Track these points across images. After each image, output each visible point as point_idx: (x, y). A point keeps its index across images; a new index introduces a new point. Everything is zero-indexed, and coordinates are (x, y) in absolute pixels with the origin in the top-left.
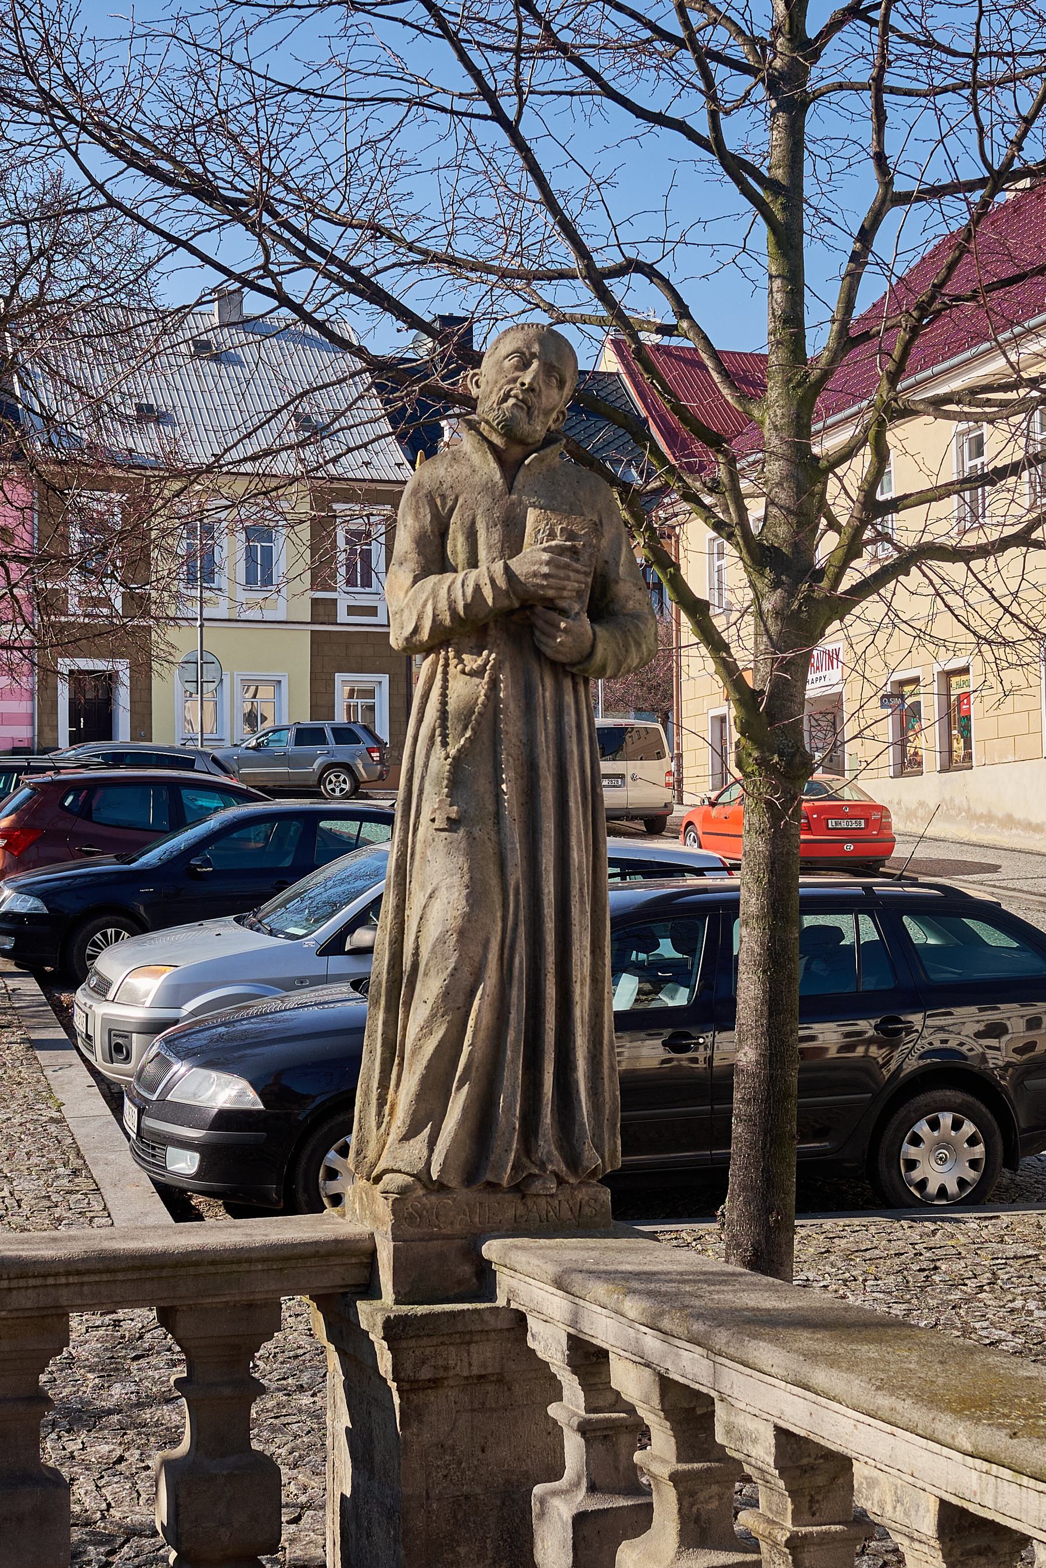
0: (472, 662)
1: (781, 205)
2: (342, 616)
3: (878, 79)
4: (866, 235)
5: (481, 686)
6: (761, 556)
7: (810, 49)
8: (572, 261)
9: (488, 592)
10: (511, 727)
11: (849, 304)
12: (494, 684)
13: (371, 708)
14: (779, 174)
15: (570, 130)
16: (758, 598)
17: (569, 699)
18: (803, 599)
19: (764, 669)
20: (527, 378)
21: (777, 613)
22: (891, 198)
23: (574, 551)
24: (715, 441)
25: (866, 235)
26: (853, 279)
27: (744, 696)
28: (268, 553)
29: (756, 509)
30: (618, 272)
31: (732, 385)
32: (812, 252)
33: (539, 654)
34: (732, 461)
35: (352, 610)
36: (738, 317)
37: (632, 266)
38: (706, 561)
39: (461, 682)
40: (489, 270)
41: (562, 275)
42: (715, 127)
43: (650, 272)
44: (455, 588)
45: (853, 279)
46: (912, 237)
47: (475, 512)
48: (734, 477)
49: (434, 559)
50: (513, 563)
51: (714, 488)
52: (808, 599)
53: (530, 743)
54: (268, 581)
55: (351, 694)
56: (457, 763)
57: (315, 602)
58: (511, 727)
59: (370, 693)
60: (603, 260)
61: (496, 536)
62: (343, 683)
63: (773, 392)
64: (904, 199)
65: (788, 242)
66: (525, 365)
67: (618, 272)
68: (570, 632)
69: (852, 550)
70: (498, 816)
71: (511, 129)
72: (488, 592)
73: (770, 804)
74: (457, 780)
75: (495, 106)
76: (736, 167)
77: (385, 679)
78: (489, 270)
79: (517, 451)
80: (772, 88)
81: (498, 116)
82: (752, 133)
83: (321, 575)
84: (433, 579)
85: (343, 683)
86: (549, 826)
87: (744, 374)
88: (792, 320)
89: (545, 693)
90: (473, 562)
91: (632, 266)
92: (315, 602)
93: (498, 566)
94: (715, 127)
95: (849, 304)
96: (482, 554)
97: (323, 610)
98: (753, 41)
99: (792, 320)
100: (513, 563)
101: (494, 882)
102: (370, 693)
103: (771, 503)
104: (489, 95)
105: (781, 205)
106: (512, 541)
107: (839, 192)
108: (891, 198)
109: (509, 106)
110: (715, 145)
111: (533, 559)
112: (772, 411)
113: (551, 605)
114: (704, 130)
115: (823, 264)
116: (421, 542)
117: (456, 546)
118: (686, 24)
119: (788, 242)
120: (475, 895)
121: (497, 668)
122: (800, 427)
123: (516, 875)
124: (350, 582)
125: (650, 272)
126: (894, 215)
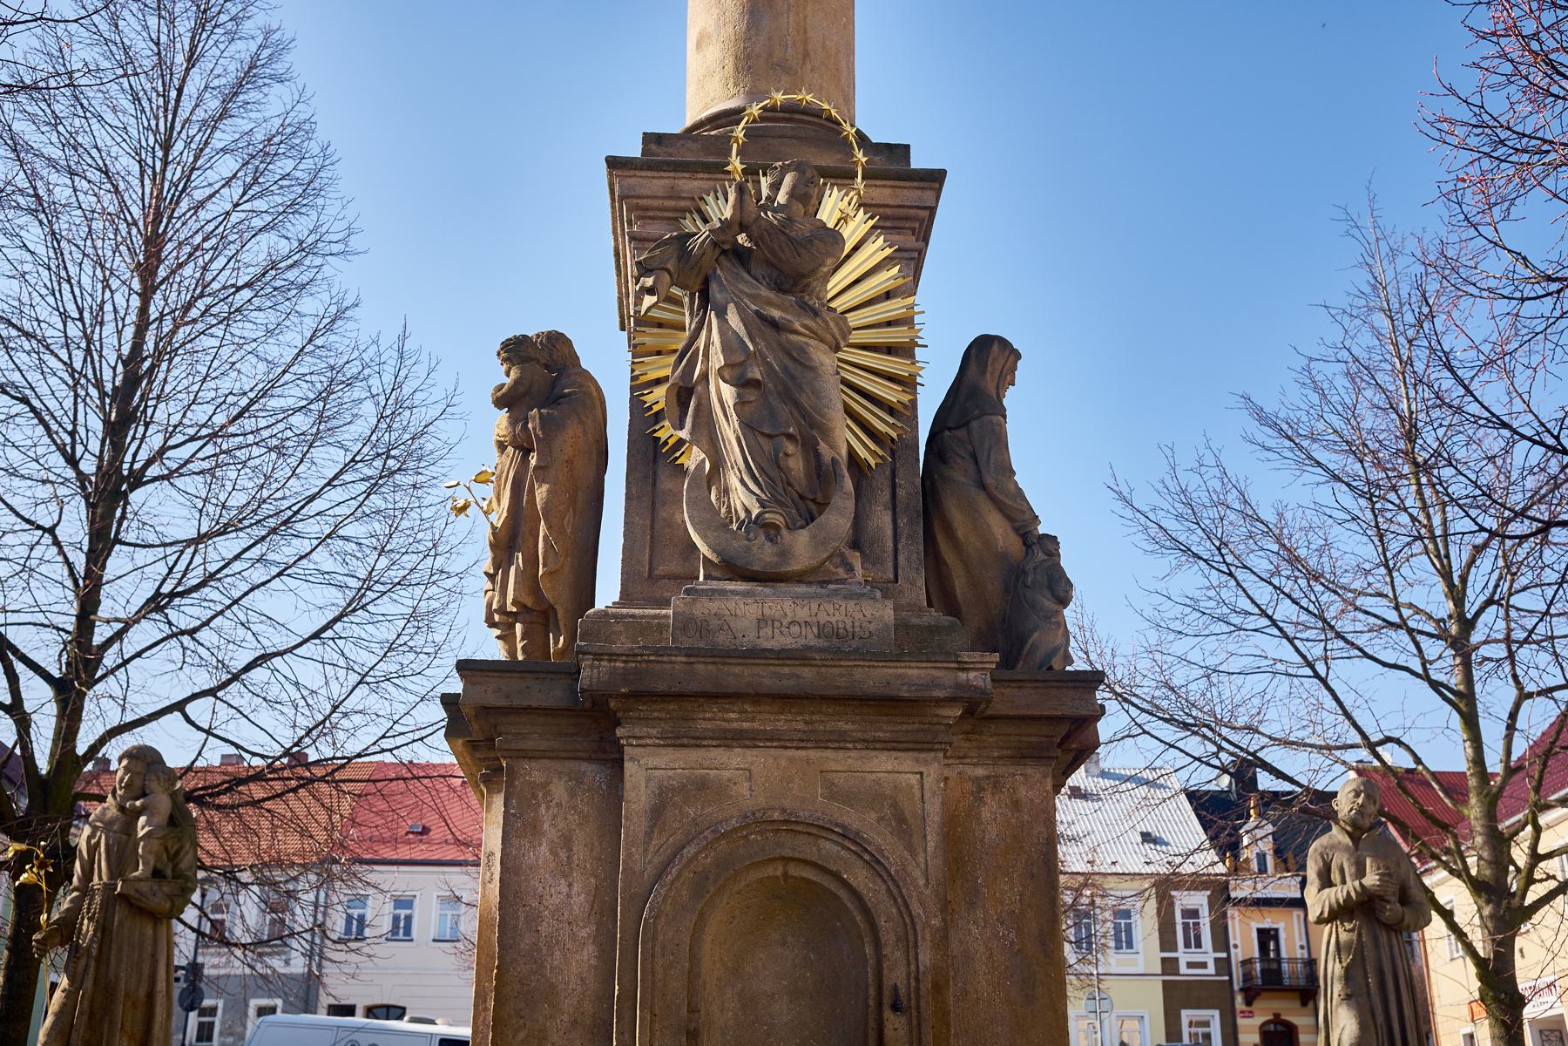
0: (1348, 926)
1: (1466, 705)
2: (1183, 969)
3: (1508, 636)
4: (1513, 716)
5: (1354, 936)
6: (1478, 887)
7: (1468, 625)
8: (1358, 739)
9: (1353, 894)
10: (1369, 953)
11: (1508, 752)
12: (1360, 935)
13: (1207, 1036)
14: (1461, 688)
15: (1348, 674)
16: (1479, 910)
17: (1394, 941)
18: (1508, 913)
19: (1489, 947)
20: (1360, 801)
21: (1492, 916)
22: (1523, 696)
23: (1390, 875)
24: (1445, 827)
25: (1513, 716)
26: (1509, 739)
27: (1480, 963)
28: (1129, 927)
29: (1472, 861)
30: (1381, 743)
31: (1451, 798)
32: (1484, 724)
33: (1378, 921)
34: (1455, 837)
35: (1190, 965)
36: (1445, 752)
37: (1388, 740)
38: (1449, 890)
39: (1344, 932)
40: (1306, 745)
41: (1352, 746)
42: (1425, 670)
43: (1398, 742)
44: (1337, 894)
45: (1509, 739)
46: (1539, 718)
47: (1341, 860)
48: (1458, 845)
49: (1326, 882)
50: (1364, 881)
51: (1448, 851)
52: (1508, 908)
53: (1379, 961)
54: (1130, 945)
55: (1191, 1024)
56: (1347, 970)
57: (1164, 960)
58: (1369, 953)
59: (1207, 1024)
60: (1374, 739)
61: (1353, 869)
62: (1186, 1015)
63: (1473, 800)
64: (1530, 695)
65: (1471, 722)
66: (1357, 795)
67: (1381, 743)
68: (1391, 910)
69: (1530, 881)
70: (1368, 993)
71: (1324, 681)
72: (1353, 894)
73: (1504, 1022)
74: (1348, 976)
75: (1314, 671)
76: (1435, 686)
77: (1216, 1013)
78: (1306, 745)
79: (1358, 833)
80: (1452, 646)
81: (1317, 675)
82: (1446, 668)
83: (1167, 942)
84: (1327, 890)
85: (1186, 1015)
86: (1392, 998)
87: (1453, 784)
88: (1478, 760)
89: (1383, 938)
90: (1344, 882)
91: (1388, 740)
92: (1164, 960)
93: (1357, 883)
94: (1425, 670)
95: (1508, 752)
96: (1348, 879)
97: (1169, 965)
98: (1438, 621)
99: (1478, 760)
100: (1364, 881)
101: (1370, 1022)
102: (1207, 1024)
103: (1480, 858)
104: (1311, 666)
105: (1466, 705)
106: (1360, 873)
107: (1494, 696)
108: (1523, 696)
109: (1321, 668)
110: (1426, 677)
111: (1371, 879)
112: (1474, 810)
113: (1382, 898)
114: (1420, 670)
115: (1492, 733)
116: (1320, 874)
117: (1335, 876)
118: (1401, 616)
119: (1471, 722)
120: (1363, 1026)
121: (1360, 928)
122: (1491, 816)
123: (1380, 1019)
124: (1187, 945)
125: (1398, 742)
126: (1527, 704)
